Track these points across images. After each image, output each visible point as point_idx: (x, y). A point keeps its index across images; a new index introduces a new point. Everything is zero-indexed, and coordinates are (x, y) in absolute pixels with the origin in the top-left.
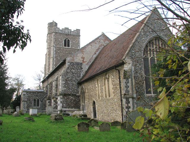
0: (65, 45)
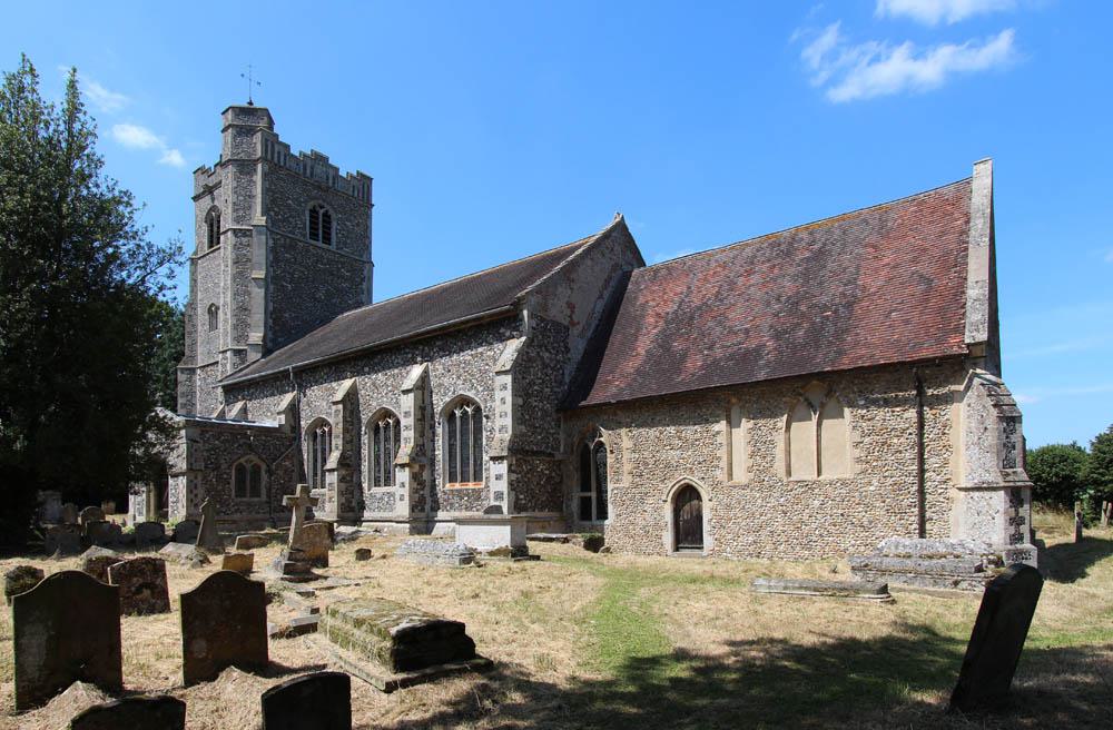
0: (314, 236)
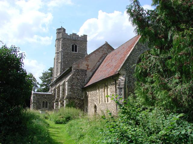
0: (73, 51)
